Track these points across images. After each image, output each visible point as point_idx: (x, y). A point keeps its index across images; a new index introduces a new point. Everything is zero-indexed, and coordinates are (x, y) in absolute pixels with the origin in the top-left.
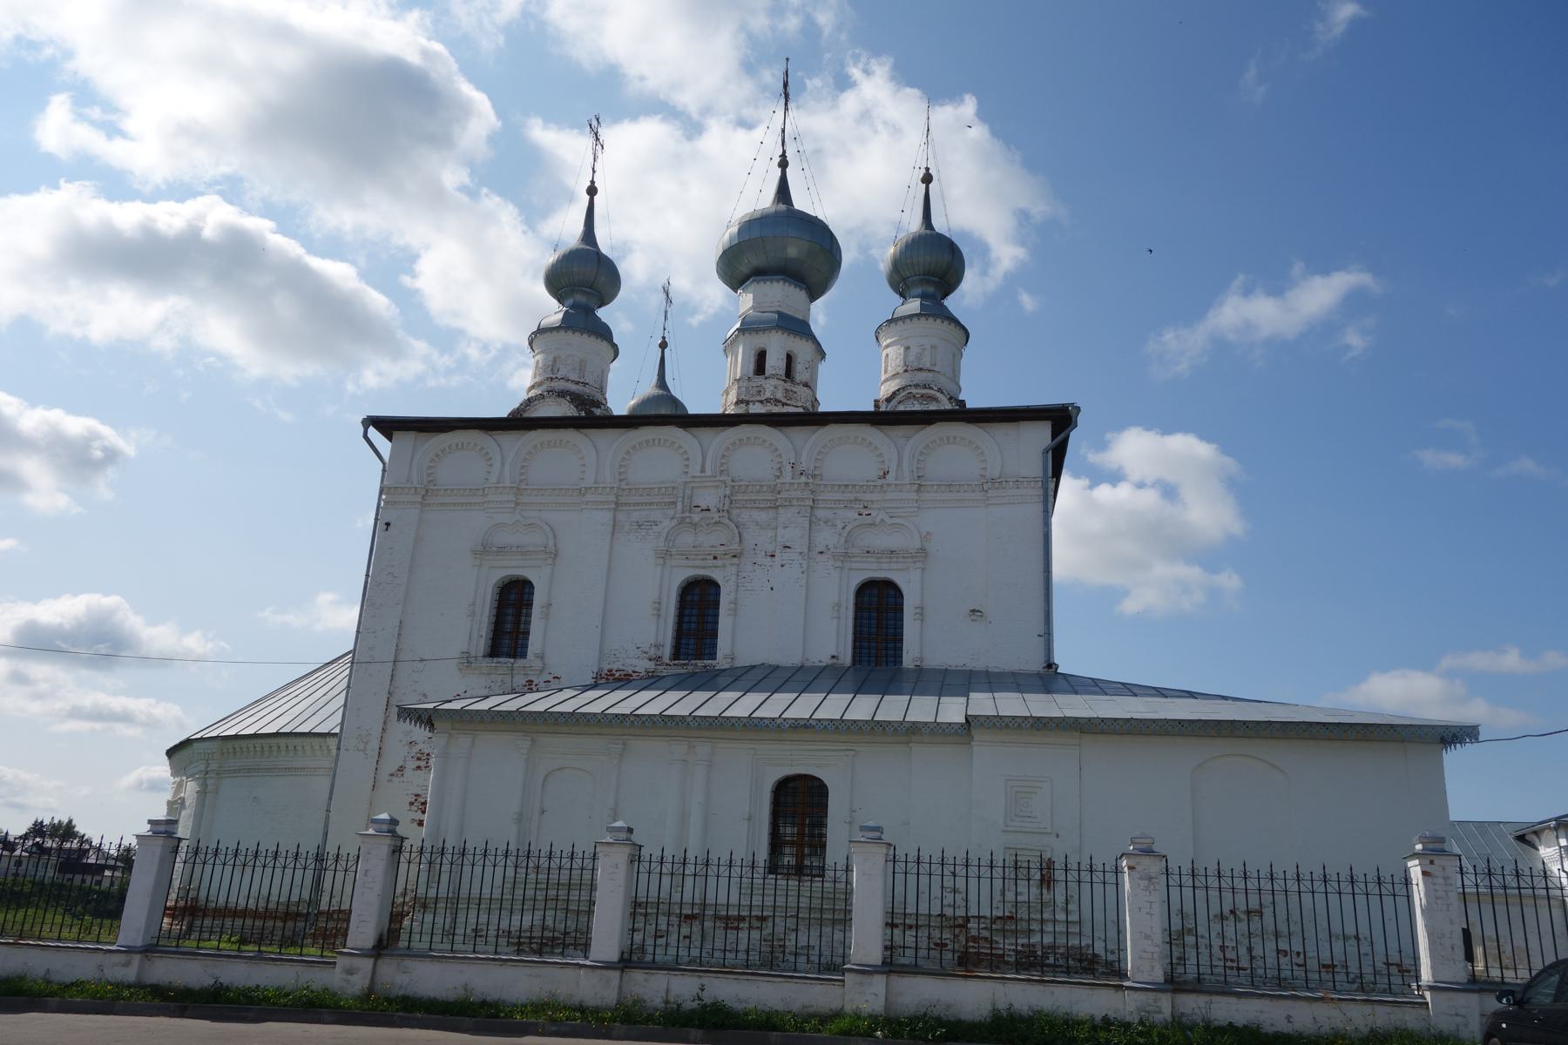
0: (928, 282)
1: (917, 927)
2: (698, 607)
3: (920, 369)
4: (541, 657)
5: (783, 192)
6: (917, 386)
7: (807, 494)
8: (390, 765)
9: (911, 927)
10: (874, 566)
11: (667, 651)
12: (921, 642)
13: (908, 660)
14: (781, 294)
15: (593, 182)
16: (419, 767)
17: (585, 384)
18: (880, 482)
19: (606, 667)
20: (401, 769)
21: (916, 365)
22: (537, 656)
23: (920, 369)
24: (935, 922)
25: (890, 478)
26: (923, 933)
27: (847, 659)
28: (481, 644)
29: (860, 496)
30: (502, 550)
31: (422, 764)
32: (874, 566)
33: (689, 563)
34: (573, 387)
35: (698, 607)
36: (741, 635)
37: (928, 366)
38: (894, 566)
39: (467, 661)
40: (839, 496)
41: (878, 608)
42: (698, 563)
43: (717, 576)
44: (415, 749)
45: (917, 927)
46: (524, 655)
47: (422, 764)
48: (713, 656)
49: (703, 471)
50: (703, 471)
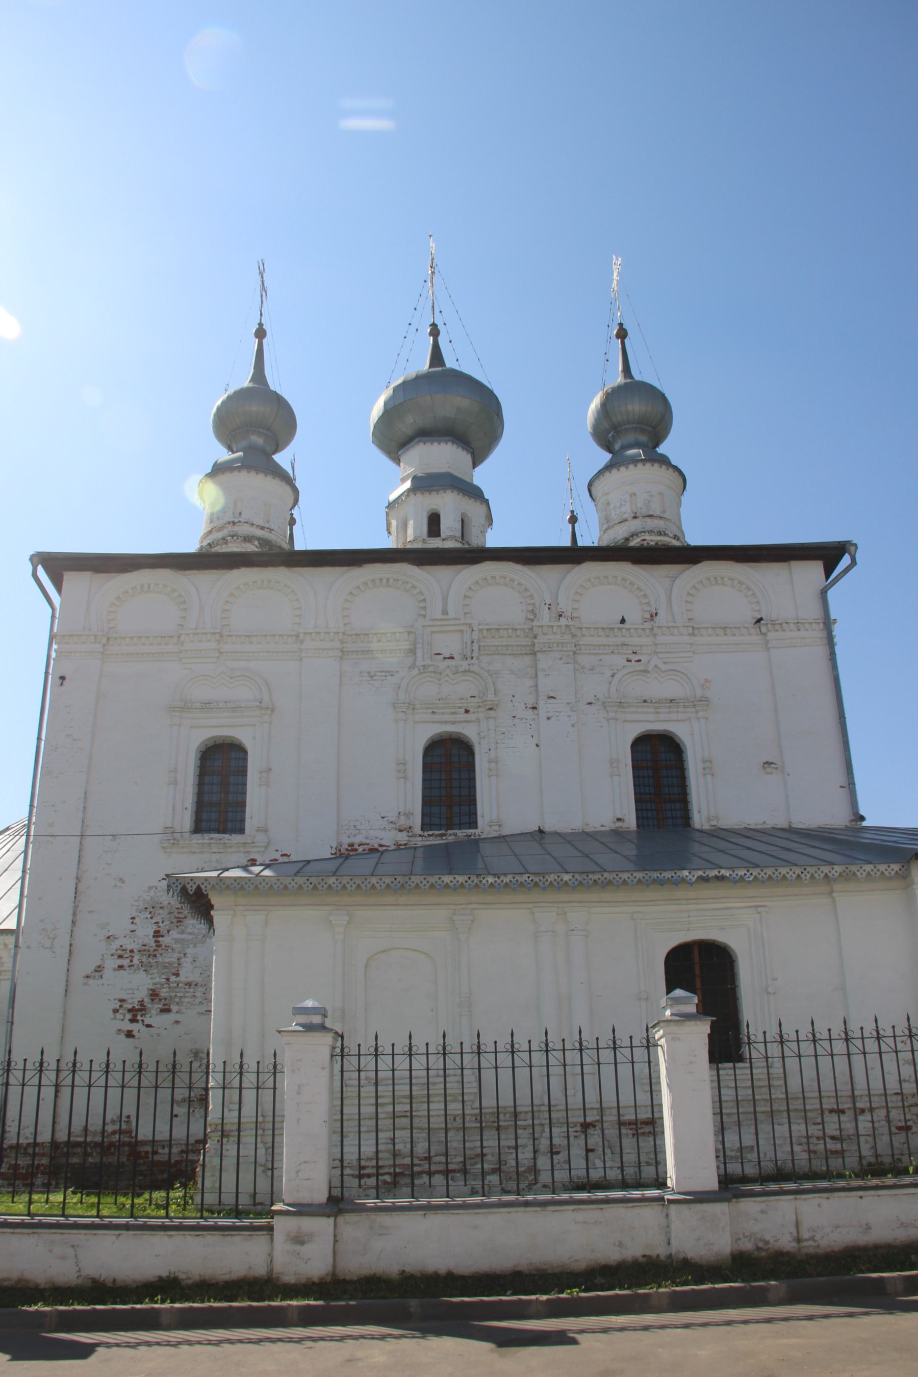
0: (643, 431)
1: (871, 1110)
2: (449, 770)
3: (650, 516)
4: (264, 830)
5: (437, 357)
6: (651, 532)
7: (567, 637)
8: (85, 964)
9: (863, 1111)
10: (651, 717)
11: (417, 821)
12: (714, 799)
13: (699, 820)
14: (442, 456)
15: (261, 325)
16: (121, 967)
17: (271, 530)
18: (648, 625)
19: (346, 841)
20: (99, 969)
21: (645, 511)
22: (259, 830)
23: (650, 516)
24: (895, 1101)
25: (661, 619)
26: (881, 1114)
27: (631, 822)
28: (186, 820)
29: (626, 640)
30: (207, 706)
31: (126, 962)
32: (651, 717)
33: (436, 717)
34: (259, 533)
35: (449, 770)
36: (506, 800)
37: (657, 512)
38: (674, 716)
39: (170, 836)
40: (604, 641)
41: (659, 764)
42: (446, 717)
43: (470, 732)
44: (115, 945)
45: (871, 1110)
46: (242, 831)
47: (126, 962)
48: (473, 824)
49: (445, 612)
50: (445, 612)
